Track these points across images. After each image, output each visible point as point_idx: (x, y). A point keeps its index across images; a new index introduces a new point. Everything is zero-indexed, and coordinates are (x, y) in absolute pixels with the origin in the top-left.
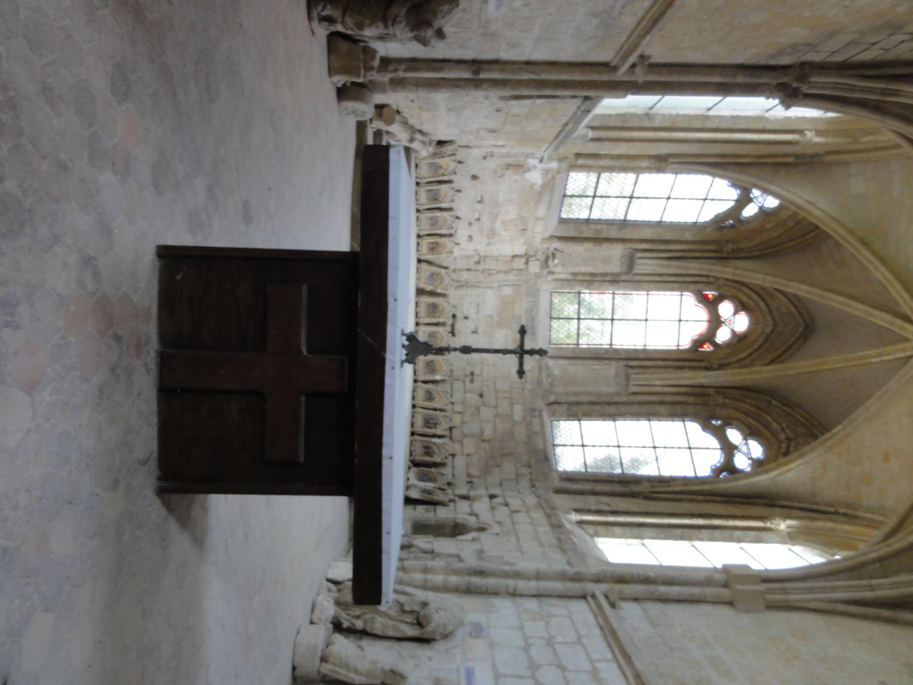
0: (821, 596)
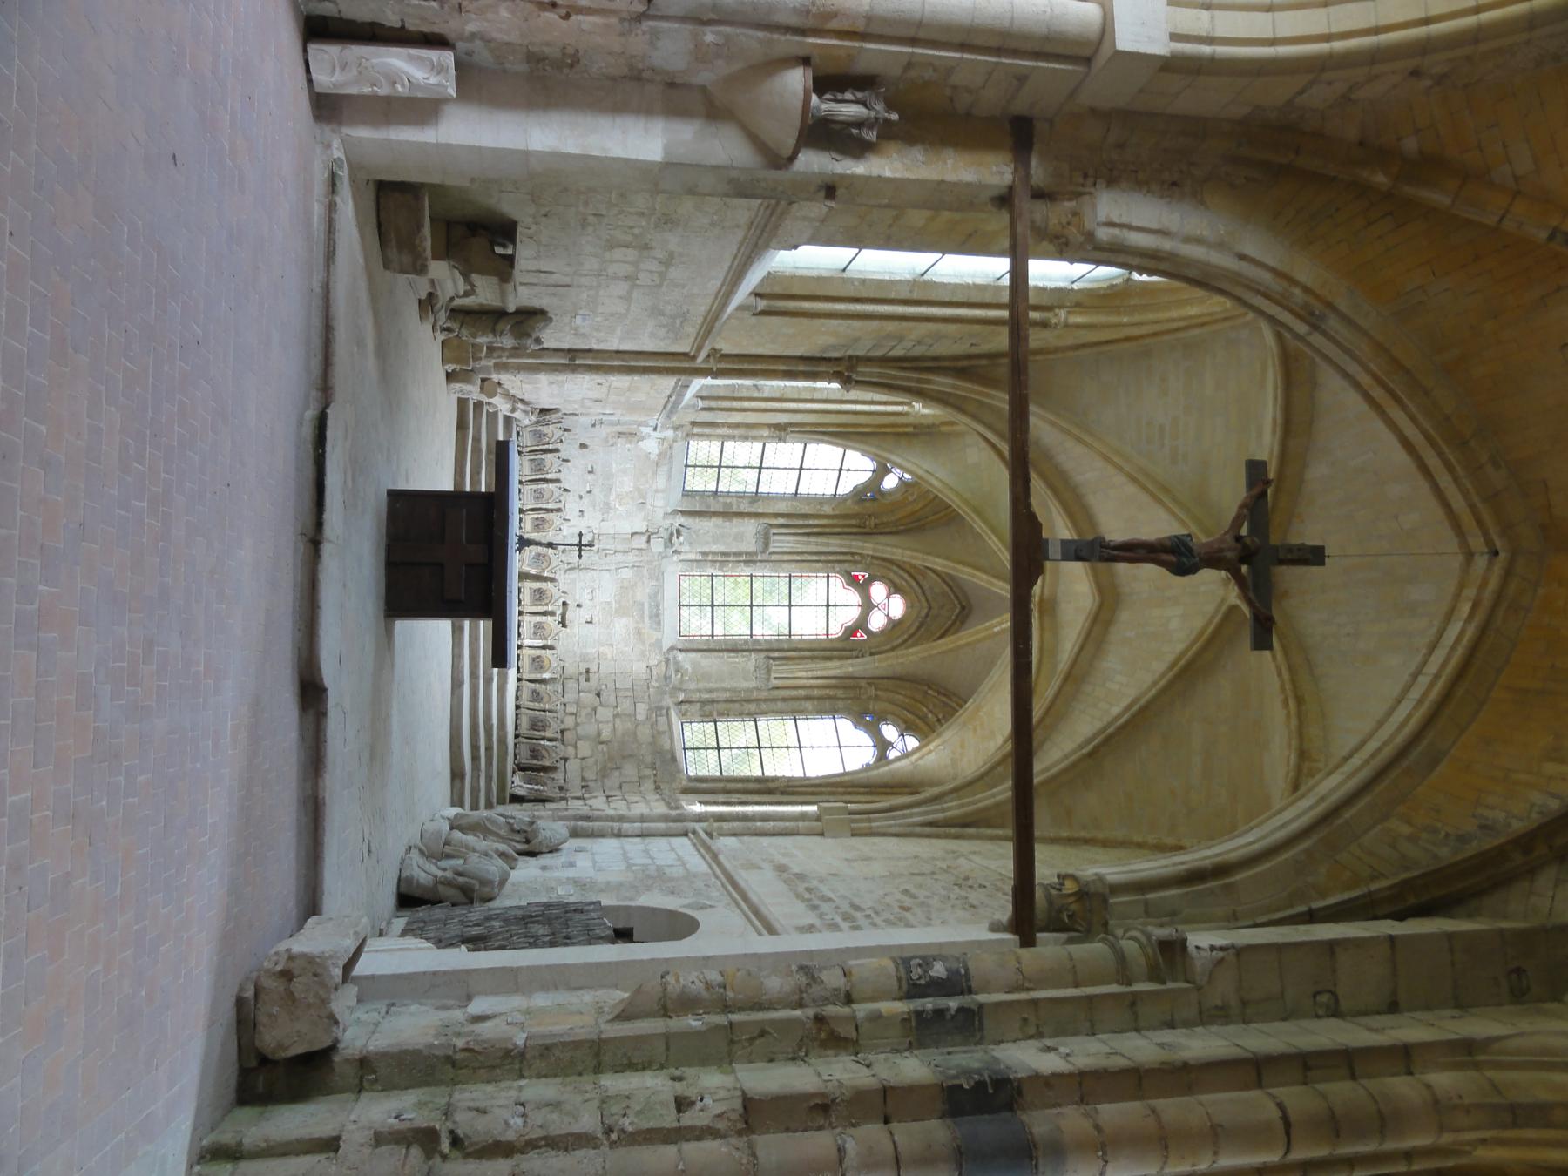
0: (901, 821)
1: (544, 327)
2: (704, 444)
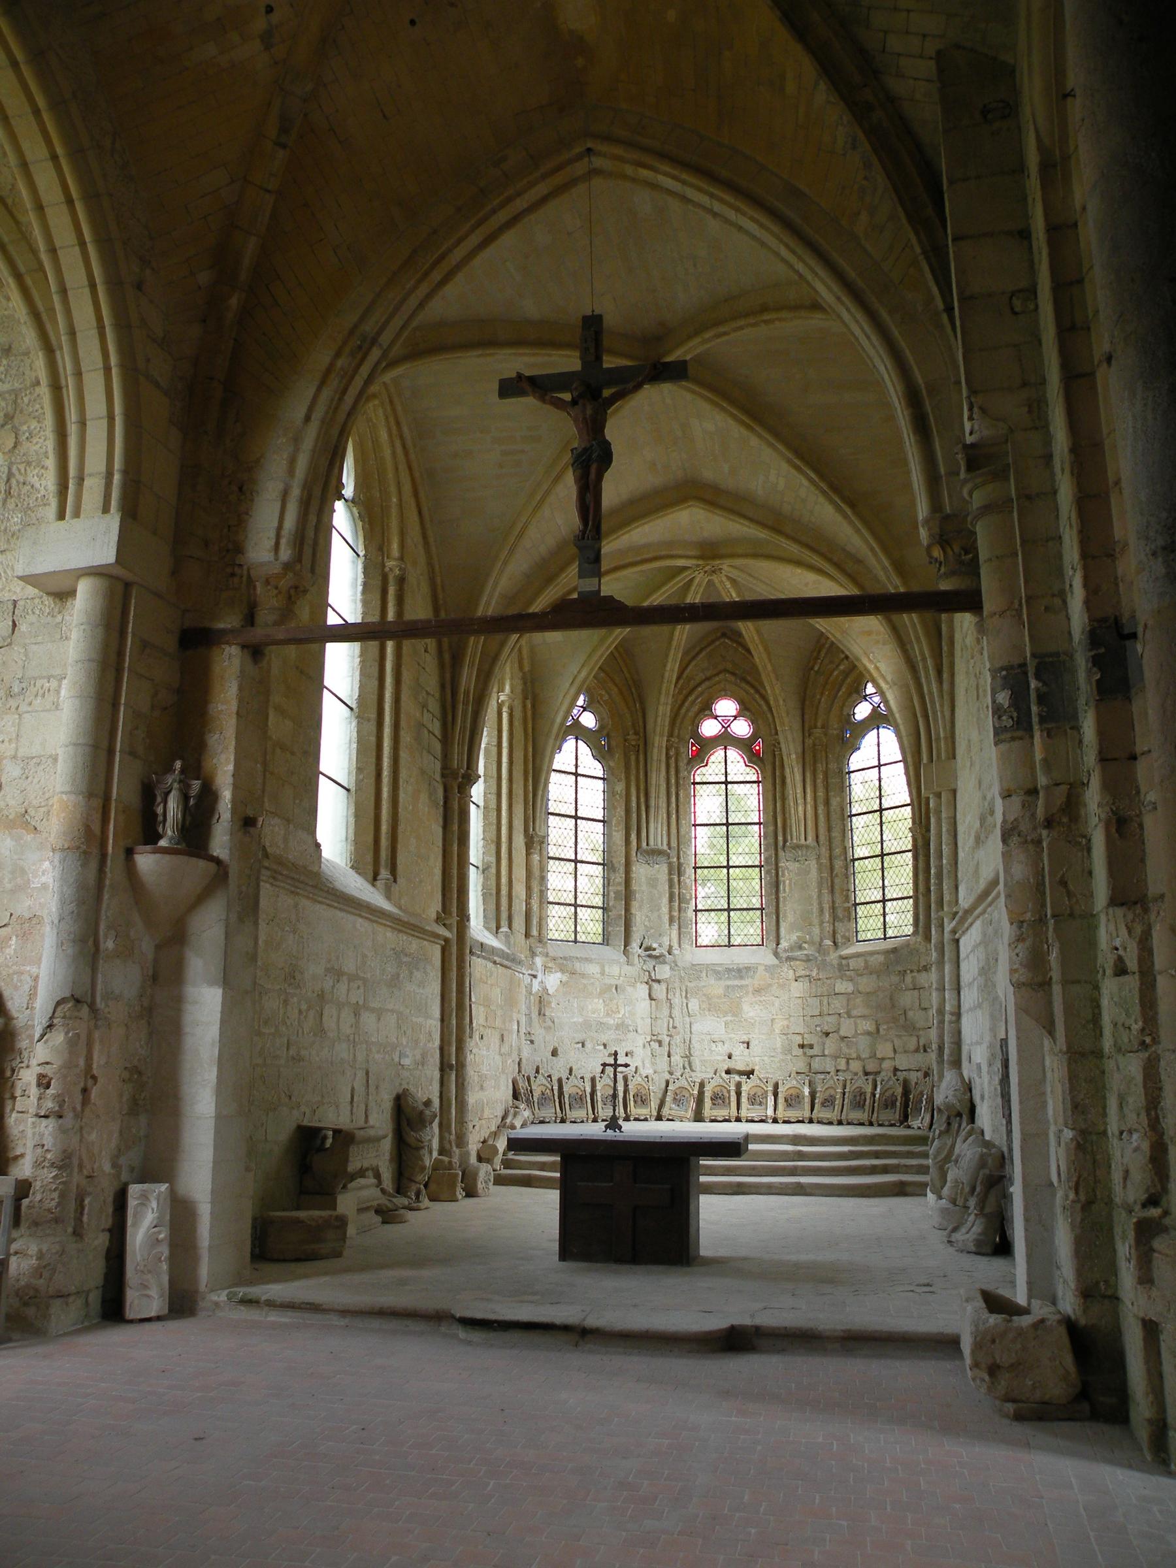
1: (413, 1097)
2: (552, 923)
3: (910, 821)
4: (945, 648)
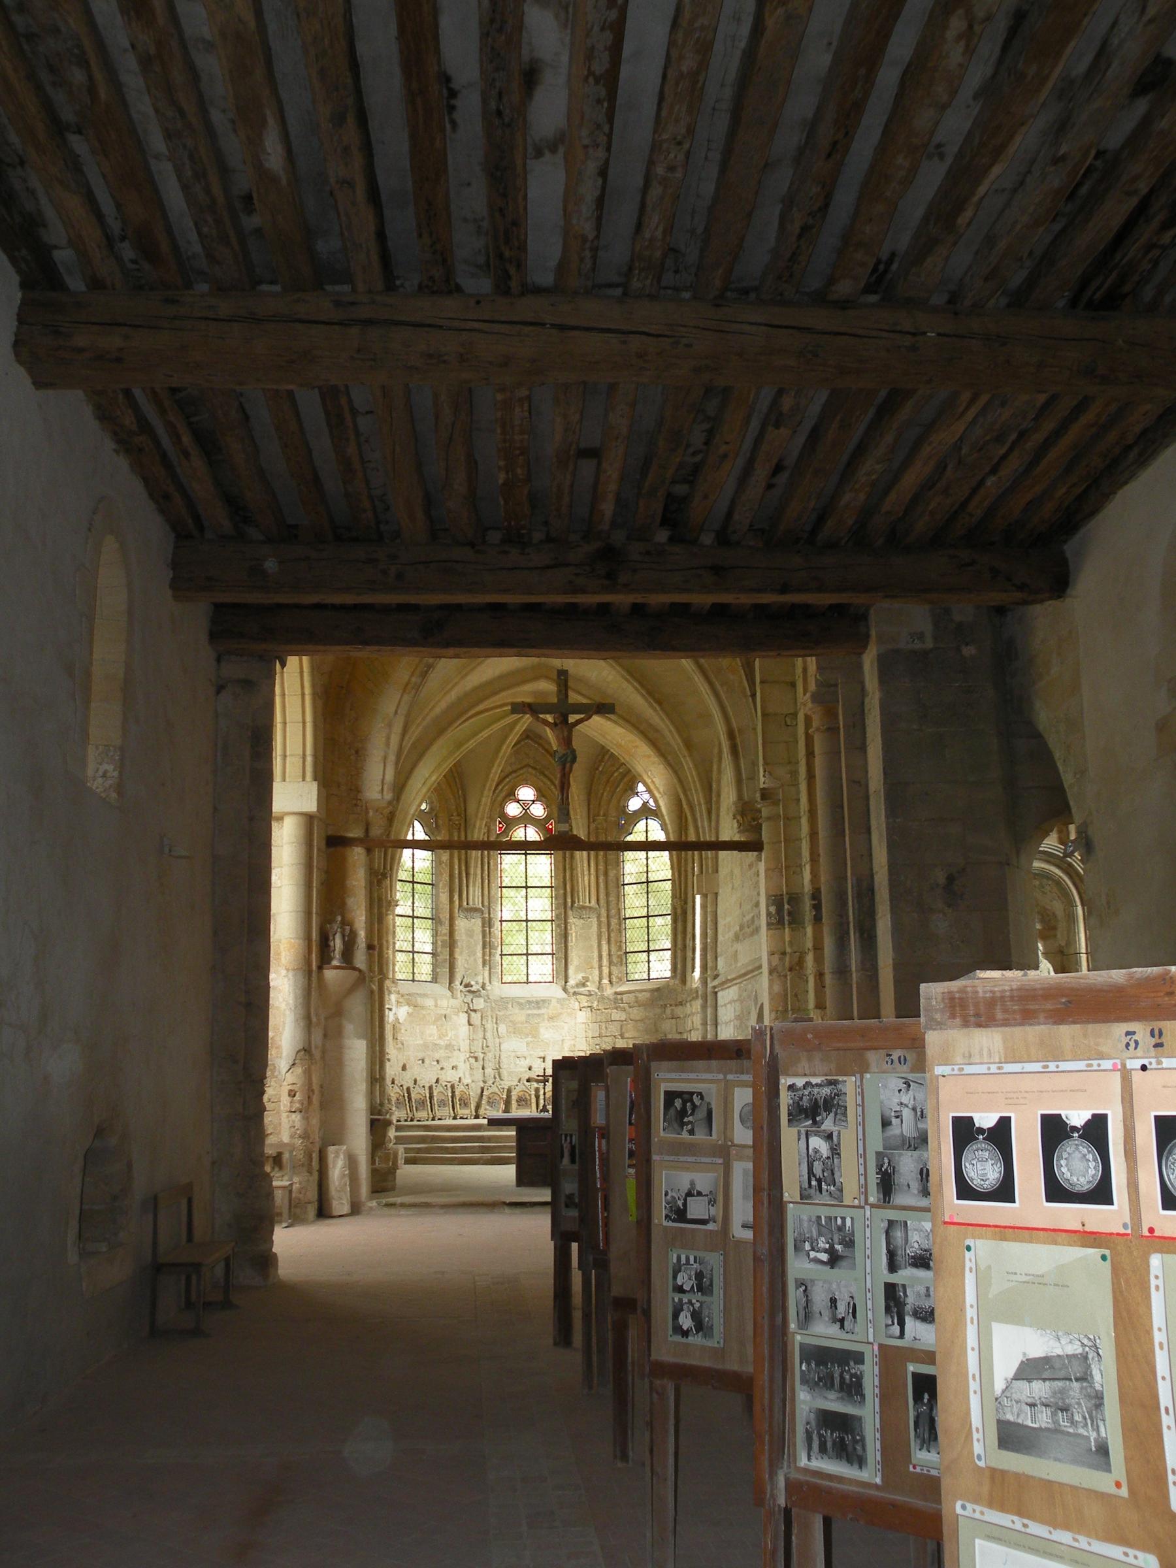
3: (670, 892)
4: (714, 799)
